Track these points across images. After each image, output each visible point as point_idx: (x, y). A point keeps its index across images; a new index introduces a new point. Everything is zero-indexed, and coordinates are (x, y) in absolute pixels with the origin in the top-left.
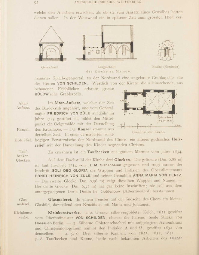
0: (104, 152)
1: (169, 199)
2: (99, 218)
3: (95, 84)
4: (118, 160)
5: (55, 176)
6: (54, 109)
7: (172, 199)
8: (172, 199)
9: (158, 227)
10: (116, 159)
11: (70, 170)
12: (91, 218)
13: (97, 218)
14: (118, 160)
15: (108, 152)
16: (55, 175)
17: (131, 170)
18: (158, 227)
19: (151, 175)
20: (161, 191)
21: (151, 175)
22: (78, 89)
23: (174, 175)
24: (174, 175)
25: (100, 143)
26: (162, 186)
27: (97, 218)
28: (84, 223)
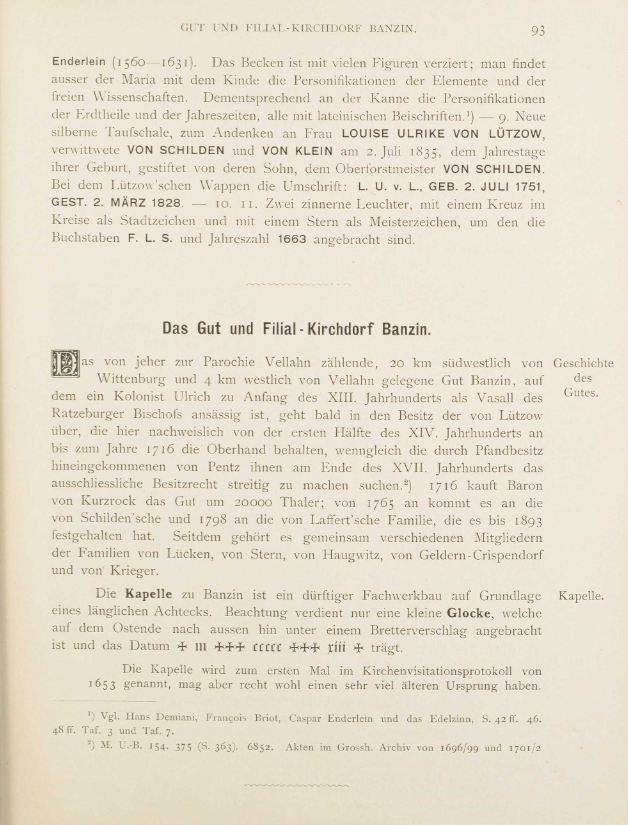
0: (479, 615)
1: (193, 329)
2: (519, 169)
3: (104, 381)
4: (458, 615)
5: (319, 152)
6: (202, 613)
7: (414, 614)
8: (414, 614)
9: (176, 166)
10: (452, 612)
11: (433, 187)
12: (492, 169)
13: (513, 169)
14: (458, 615)
15: (370, 720)
16: (319, 150)
17: (331, 593)
18: (176, 166)
19: (129, 203)
20: (91, 238)
21: (129, 203)
22: (247, 187)
23: (215, 149)
24: (215, 151)
25: (145, 638)
26: (396, 152)
27: (513, 169)
28: (68, 133)
